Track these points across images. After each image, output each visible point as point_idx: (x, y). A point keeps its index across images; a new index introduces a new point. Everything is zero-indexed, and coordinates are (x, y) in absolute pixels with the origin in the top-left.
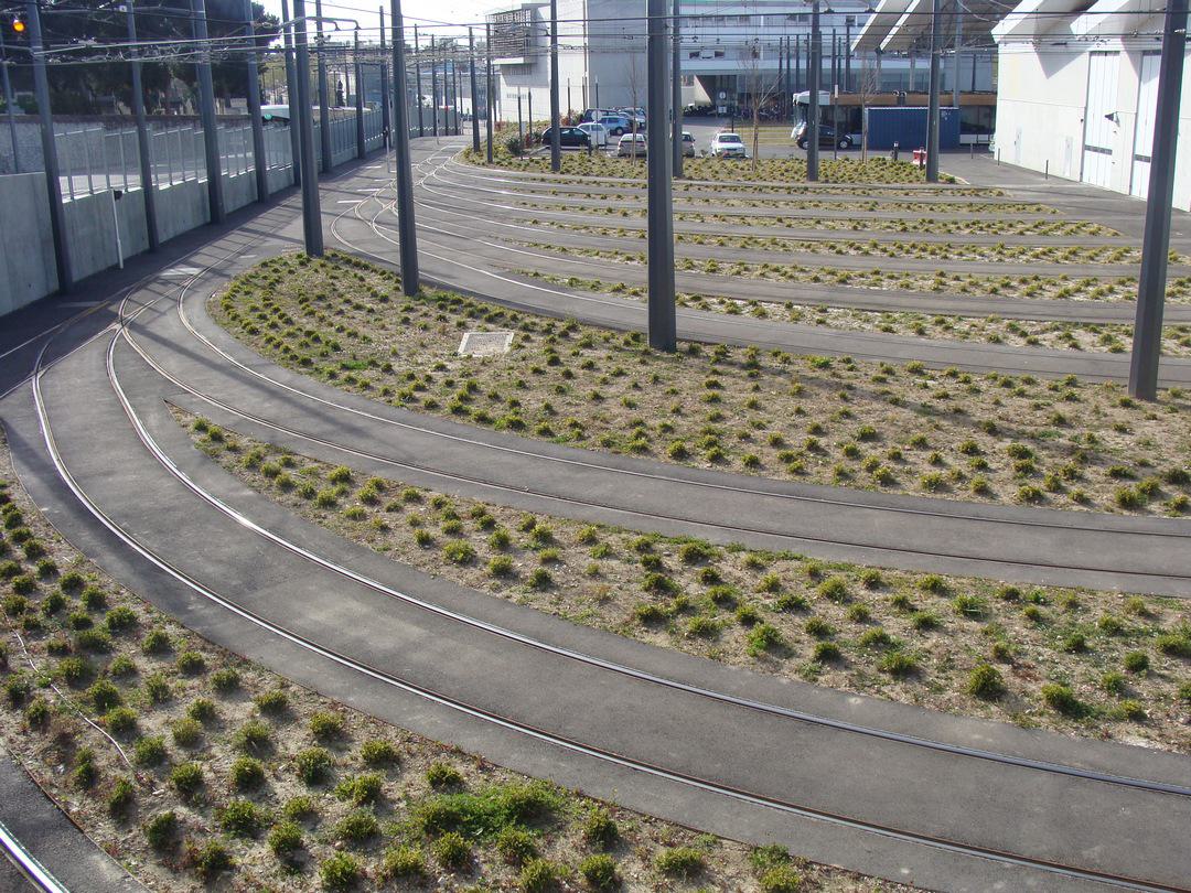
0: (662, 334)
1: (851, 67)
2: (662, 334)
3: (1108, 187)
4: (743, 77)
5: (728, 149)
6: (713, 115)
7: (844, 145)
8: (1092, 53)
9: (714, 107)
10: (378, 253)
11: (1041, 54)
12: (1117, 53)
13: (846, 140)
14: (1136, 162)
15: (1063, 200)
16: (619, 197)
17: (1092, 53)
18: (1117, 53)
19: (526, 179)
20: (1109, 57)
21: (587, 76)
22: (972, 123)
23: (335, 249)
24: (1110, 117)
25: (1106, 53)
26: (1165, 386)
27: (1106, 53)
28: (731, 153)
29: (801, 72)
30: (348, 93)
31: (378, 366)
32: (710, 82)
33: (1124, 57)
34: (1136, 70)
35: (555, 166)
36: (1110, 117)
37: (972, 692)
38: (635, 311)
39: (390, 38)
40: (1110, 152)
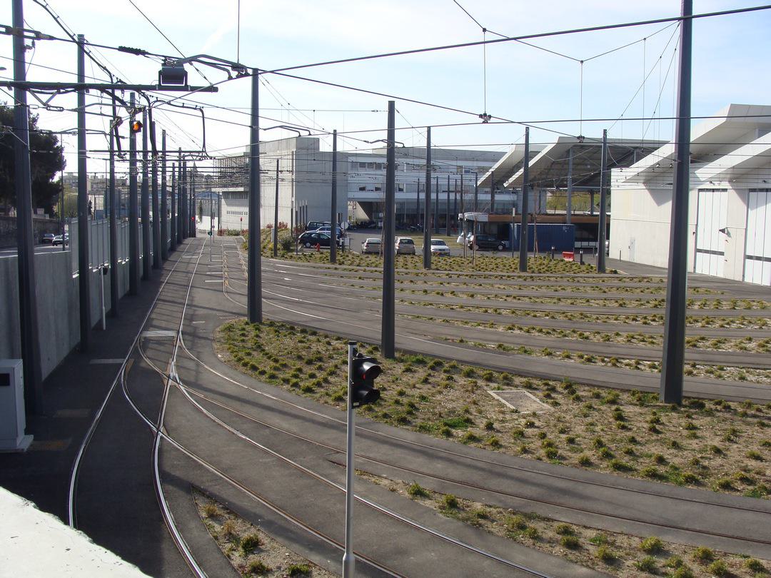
0: (673, 392)
1: (420, 198)
2: (673, 392)
3: (721, 275)
4: (377, 203)
5: (440, 250)
6: (375, 228)
7: (501, 248)
8: (700, 190)
9: (371, 222)
10: (303, 322)
11: (652, 191)
12: (725, 190)
13: (502, 244)
14: (747, 260)
15: (712, 285)
16: (412, 281)
17: (700, 190)
18: (725, 190)
19: (299, 266)
20: (715, 193)
21: (294, 200)
22: (593, 231)
23: (304, 325)
24: (723, 231)
25: (713, 190)
26: (688, 362)
27: (713, 190)
28: (443, 252)
29: (451, 201)
30: (95, 207)
31: (672, 467)
32: (367, 206)
33: (732, 194)
34: (744, 201)
35: (333, 260)
36: (723, 231)
37: (398, 420)
38: (653, 378)
39: (158, 177)
40: (722, 254)
